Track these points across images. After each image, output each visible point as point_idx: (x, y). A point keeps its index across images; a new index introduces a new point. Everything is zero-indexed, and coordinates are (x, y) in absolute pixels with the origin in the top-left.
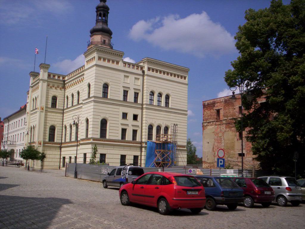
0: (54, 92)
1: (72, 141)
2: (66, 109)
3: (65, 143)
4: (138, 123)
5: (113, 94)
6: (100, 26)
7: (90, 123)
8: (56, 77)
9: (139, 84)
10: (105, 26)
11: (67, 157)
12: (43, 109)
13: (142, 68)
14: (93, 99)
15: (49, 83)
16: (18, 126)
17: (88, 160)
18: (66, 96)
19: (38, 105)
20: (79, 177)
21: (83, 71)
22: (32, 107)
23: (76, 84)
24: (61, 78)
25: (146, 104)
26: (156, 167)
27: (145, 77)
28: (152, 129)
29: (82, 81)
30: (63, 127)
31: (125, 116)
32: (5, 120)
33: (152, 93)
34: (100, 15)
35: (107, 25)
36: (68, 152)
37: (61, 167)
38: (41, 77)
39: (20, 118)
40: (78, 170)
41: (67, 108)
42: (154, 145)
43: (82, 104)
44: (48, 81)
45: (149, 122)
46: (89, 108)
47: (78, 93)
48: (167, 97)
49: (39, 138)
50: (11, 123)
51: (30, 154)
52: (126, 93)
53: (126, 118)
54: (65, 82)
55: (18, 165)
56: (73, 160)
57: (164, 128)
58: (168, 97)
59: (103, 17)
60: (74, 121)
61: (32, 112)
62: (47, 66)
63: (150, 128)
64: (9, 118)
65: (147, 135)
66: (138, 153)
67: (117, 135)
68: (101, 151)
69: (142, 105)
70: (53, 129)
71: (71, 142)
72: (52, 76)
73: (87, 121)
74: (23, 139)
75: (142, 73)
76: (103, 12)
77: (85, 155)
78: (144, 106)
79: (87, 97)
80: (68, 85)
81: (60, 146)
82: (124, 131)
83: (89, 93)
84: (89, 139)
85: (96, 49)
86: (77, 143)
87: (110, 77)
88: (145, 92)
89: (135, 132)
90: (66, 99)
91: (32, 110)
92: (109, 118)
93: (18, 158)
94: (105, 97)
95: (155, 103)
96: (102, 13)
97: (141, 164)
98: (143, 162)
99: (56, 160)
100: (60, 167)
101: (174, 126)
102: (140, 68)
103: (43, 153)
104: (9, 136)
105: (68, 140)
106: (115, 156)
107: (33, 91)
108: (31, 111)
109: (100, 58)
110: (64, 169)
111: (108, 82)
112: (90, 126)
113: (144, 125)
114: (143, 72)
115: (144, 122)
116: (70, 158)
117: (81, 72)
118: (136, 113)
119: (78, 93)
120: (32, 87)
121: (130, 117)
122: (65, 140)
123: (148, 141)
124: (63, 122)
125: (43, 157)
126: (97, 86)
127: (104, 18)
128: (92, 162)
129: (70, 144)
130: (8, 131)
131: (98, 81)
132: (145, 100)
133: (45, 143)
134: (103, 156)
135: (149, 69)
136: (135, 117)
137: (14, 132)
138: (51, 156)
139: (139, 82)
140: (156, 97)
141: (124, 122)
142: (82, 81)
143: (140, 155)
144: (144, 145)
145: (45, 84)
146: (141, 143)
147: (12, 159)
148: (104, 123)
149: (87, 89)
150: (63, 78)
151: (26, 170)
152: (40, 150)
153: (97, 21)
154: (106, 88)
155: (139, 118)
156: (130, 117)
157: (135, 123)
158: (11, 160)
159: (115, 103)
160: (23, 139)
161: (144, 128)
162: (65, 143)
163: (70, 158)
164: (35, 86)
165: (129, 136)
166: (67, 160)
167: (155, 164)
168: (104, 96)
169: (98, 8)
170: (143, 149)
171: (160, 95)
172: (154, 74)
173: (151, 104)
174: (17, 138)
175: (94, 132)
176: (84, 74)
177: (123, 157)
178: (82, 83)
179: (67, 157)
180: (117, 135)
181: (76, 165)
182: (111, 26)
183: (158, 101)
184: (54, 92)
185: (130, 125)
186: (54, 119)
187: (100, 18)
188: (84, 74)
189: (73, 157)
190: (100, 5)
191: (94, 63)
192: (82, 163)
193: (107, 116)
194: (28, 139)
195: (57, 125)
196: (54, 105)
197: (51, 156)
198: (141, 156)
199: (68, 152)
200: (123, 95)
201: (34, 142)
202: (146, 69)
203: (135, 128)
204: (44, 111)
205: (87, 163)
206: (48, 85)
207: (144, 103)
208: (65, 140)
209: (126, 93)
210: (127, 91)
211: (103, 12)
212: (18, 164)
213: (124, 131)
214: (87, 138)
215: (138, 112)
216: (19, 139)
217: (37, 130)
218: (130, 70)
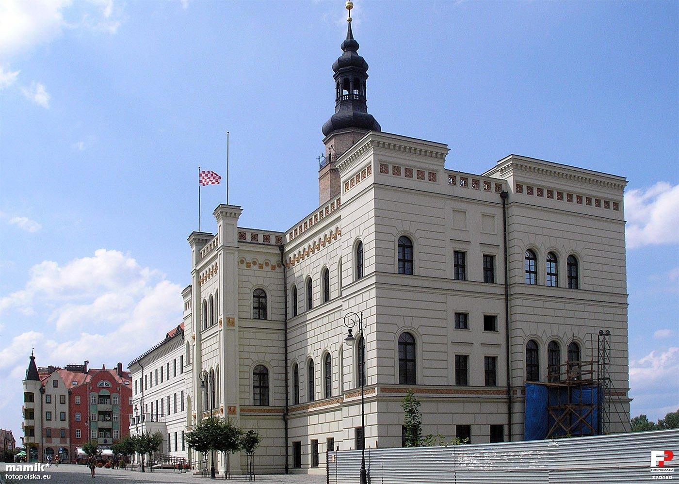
6: (349, 112)
28: (537, 350)
31: (462, 320)
32: (132, 368)
33: (532, 255)
37: (289, 467)
44: (239, 251)
45: (528, 333)
48: (573, 262)
52: (460, 257)
53: (466, 327)
54: (287, 250)
57: (569, 346)
58: (573, 262)
60: (350, 331)
63: (533, 348)
64: (142, 362)
65: (525, 369)
67: (443, 373)
75: (500, 200)
82: (462, 362)
89: (491, 362)
92: (422, 331)
93: (179, 453)
94: (404, 273)
95: (544, 279)
96: (350, 77)
101: (601, 338)
104: (145, 403)
109: (383, 168)
111: (412, 231)
121: (476, 322)
123: (528, 385)
124: (286, 353)
127: (356, 92)
130: (142, 391)
136: (490, 323)
140: (544, 266)
143: (507, 423)
144: (196, 463)
148: (408, 342)
154: (408, 247)
155: (500, 323)
157: (490, 336)
165: (476, 374)
168: (401, 270)
178: (335, 244)
180: (443, 373)
181: (363, 454)
182: (373, 108)
187: (345, 92)
203: (491, 352)
204: (236, 328)
209: (460, 257)
212: (180, 467)
213: (462, 362)
215: (496, 308)
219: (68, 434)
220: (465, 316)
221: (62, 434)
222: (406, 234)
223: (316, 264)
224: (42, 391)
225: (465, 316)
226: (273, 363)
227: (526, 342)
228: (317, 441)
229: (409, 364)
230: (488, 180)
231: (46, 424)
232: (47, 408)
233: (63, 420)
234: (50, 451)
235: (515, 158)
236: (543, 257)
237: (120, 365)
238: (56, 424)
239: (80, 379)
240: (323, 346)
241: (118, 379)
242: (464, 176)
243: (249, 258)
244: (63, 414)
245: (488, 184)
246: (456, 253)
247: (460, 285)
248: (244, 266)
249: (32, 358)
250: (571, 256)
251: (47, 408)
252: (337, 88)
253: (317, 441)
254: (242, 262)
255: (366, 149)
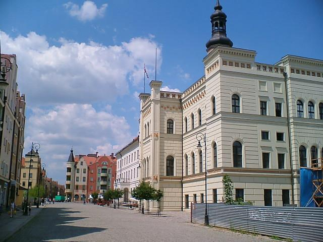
0: (169, 115)
1: (189, 174)
2: (185, 134)
3: (187, 176)
4: (284, 144)
5: (246, 108)
6: (217, 37)
7: (218, 148)
8: (171, 97)
9: (281, 92)
10: (223, 37)
11: (191, 195)
12: (156, 179)
13: (282, 70)
14: (220, 115)
15: (162, 103)
16: (131, 160)
17: (219, 198)
18: (184, 118)
19: (151, 133)
20: (210, 224)
21: (204, 83)
22: (144, 135)
23: (196, 100)
24: (177, 97)
25: (294, 118)
26: (317, 206)
27: (289, 82)
29: (204, 96)
30: (183, 156)
31: (265, 135)
33: (300, 103)
34: (216, 25)
35: (226, 36)
36: (191, 189)
38: (152, 98)
39: (133, 152)
40: (209, 213)
41: (187, 132)
42: (310, 174)
43: (206, 124)
46: (215, 128)
47: (200, 112)
49: (154, 171)
50: (123, 158)
51: (144, 192)
55: (131, 207)
56: (199, 199)
59: (220, 26)
61: (144, 142)
62: (158, 84)
63: (303, 150)
66: (288, 187)
68: (236, 185)
69: (288, 118)
70: (170, 160)
71: (194, 175)
72: (165, 96)
73: (214, 145)
74: (137, 175)
76: (219, 21)
77: (215, 191)
78: (291, 121)
79: (211, 115)
80: (185, 104)
81: (181, 182)
82: (266, 157)
83: (214, 109)
84: (220, 169)
85: (219, 51)
86: (205, 176)
87: (240, 85)
88: (290, 101)
89: (281, 157)
90: (184, 121)
91: (144, 138)
95: (306, 115)
96: (218, 21)
97: (293, 200)
98: (296, 198)
99: (177, 199)
100: (182, 208)
102: (279, 71)
103: (159, 191)
105: (190, 173)
106: (256, 191)
107: (143, 117)
108: (144, 140)
109: (224, 63)
110: (189, 210)
112: (219, 152)
113: (293, 146)
114: (285, 75)
115: (293, 142)
116: (195, 195)
117: (201, 85)
118: (280, 131)
119: (200, 112)
120: (143, 111)
121: (273, 136)
122: (187, 173)
125: (159, 196)
126: (224, 98)
127: (221, 28)
128: (229, 201)
129: (194, 178)
131: (225, 91)
132: (291, 112)
133: (162, 178)
134: (240, 192)
135: (292, 71)
136: (280, 137)
137: (128, 167)
138: (170, 195)
139: (281, 90)
140: (306, 108)
141: (265, 143)
142: (204, 96)
145: (158, 106)
146: (291, 171)
147: (126, 200)
148: (237, 147)
149: (211, 103)
150: (180, 96)
151: (140, 213)
152: (157, 187)
153: (213, 32)
154: (237, 99)
155: (285, 137)
156: (273, 136)
157: (280, 144)
158: (125, 201)
159: (250, 119)
160: (137, 175)
161: (293, 150)
162: (187, 176)
163: (195, 195)
164: (146, 110)
165: (273, 163)
166: (191, 199)
167: (313, 201)
168: (234, 111)
169: (213, 18)
170: (295, 179)
171: (311, 104)
172: (300, 76)
173: (300, 117)
174: (130, 175)
175: (225, 159)
176: (205, 86)
177: (268, 193)
179: (191, 195)
182: (229, 35)
183: (309, 112)
184: (169, 115)
185: (274, 148)
186: (171, 148)
187: (216, 28)
188: (205, 86)
189: (198, 194)
190: (215, 13)
191: (218, 68)
192: (212, 202)
193: (240, 138)
194: (141, 176)
195: (176, 155)
196: (170, 130)
197: (170, 195)
198: (293, 189)
199: (191, 189)
200: (260, 108)
201: (148, 178)
202: (288, 71)
205: (218, 202)
206: (162, 107)
207: (291, 116)
208: (187, 173)
210: (265, 103)
211: (219, 21)
212: (131, 206)
213: (266, 157)
214: (216, 168)
215: (283, 129)
216: (133, 176)
217: (151, 161)
218: (267, 73)
219: (86, 188)
220: (267, 133)
221: (83, 188)
222: (312, 101)
223: (196, 107)
224: (75, 167)
225: (267, 133)
226: (176, 155)
227: (299, 146)
228: (188, 195)
229: (303, 153)
230: (277, 67)
231: (76, 183)
232: (77, 175)
233: (84, 181)
234: (77, 196)
235: (290, 56)
236: (306, 105)
237: (113, 154)
238: (81, 183)
239: (93, 160)
240: (191, 149)
241: (111, 161)
242: (271, 66)
243: (165, 105)
244: (84, 178)
245: (277, 69)
246: (262, 102)
247: (235, 116)
248: (163, 109)
249: (72, 151)
250: (310, 102)
251: (77, 175)
252: (213, 26)
253: (188, 195)
254: (162, 107)
255: (216, 54)
